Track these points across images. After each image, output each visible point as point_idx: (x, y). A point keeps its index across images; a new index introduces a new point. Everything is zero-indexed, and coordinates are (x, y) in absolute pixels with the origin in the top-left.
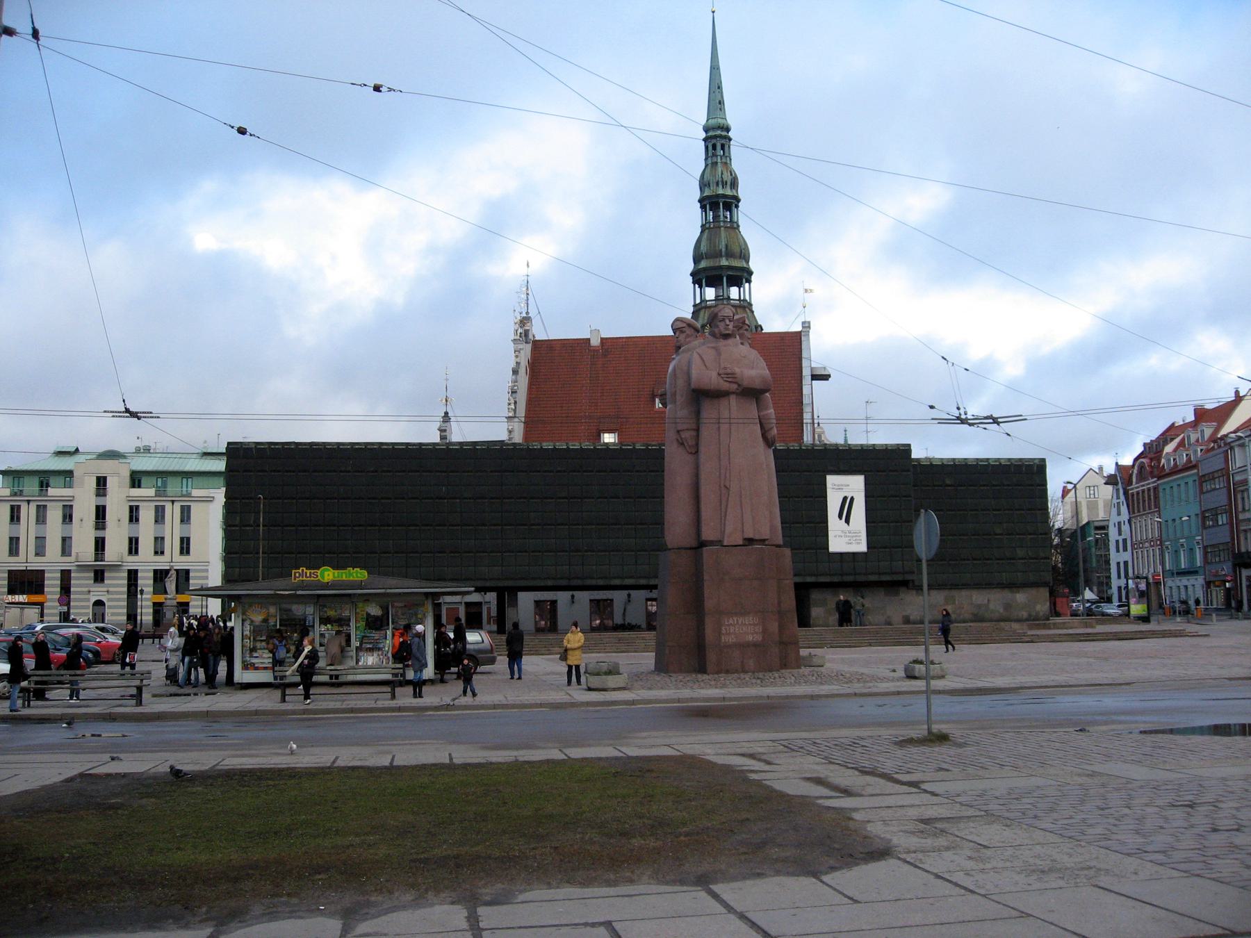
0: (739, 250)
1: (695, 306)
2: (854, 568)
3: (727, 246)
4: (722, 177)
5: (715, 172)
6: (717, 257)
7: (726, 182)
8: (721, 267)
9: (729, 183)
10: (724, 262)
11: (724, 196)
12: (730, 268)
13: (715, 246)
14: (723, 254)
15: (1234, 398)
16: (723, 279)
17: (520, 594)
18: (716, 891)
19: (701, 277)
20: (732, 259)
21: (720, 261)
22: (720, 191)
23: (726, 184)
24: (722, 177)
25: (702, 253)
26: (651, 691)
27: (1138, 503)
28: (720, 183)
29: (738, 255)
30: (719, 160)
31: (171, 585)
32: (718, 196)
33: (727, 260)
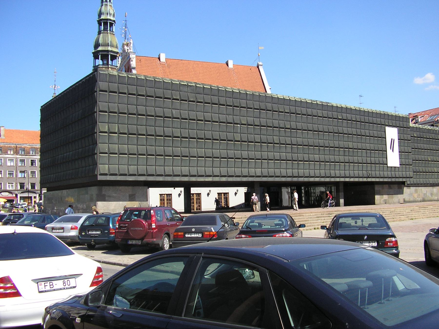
0: (116, 45)
2: (297, 141)
3: (111, 41)
4: (109, 11)
5: (106, 9)
6: (106, 46)
7: (111, 14)
8: (108, 51)
9: (112, 15)
10: (110, 48)
11: (110, 20)
12: (112, 51)
13: (105, 41)
14: (109, 45)
15: (215, 210)
16: (109, 56)
17: (184, 211)
18: (217, 264)
20: (113, 48)
21: (107, 48)
22: (109, 17)
23: (111, 15)
24: (109, 11)
25: (100, 44)
26: (144, 280)
27: (300, 219)
28: (109, 14)
29: (115, 46)
30: (108, 4)
31: (31, 203)
32: (107, 20)
33: (111, 48)
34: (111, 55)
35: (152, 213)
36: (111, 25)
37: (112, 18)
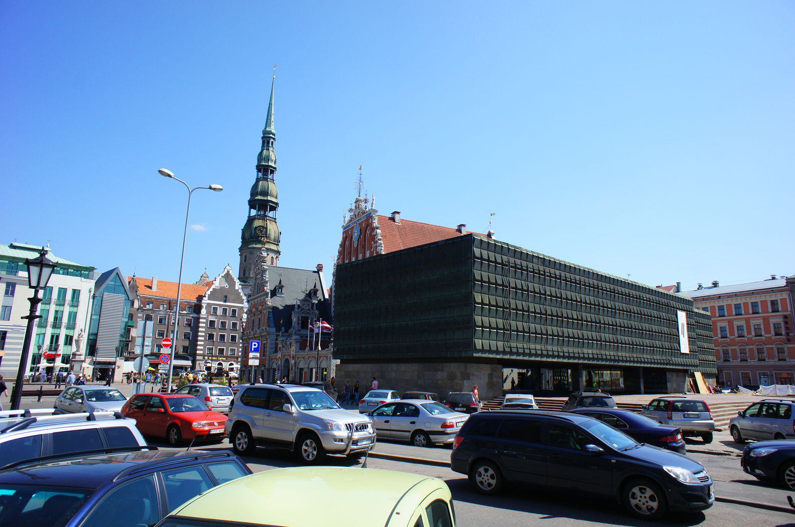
1: (249, 217)
19: (252, 204)
34: (270, 205)
35: (256, 350)
36: (272, 172)
37: (273, 165)
